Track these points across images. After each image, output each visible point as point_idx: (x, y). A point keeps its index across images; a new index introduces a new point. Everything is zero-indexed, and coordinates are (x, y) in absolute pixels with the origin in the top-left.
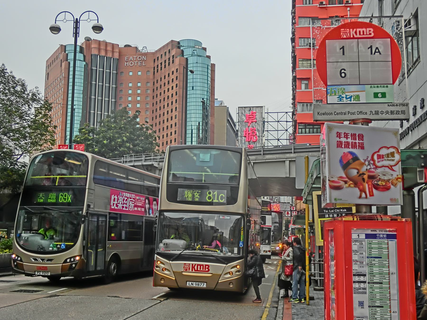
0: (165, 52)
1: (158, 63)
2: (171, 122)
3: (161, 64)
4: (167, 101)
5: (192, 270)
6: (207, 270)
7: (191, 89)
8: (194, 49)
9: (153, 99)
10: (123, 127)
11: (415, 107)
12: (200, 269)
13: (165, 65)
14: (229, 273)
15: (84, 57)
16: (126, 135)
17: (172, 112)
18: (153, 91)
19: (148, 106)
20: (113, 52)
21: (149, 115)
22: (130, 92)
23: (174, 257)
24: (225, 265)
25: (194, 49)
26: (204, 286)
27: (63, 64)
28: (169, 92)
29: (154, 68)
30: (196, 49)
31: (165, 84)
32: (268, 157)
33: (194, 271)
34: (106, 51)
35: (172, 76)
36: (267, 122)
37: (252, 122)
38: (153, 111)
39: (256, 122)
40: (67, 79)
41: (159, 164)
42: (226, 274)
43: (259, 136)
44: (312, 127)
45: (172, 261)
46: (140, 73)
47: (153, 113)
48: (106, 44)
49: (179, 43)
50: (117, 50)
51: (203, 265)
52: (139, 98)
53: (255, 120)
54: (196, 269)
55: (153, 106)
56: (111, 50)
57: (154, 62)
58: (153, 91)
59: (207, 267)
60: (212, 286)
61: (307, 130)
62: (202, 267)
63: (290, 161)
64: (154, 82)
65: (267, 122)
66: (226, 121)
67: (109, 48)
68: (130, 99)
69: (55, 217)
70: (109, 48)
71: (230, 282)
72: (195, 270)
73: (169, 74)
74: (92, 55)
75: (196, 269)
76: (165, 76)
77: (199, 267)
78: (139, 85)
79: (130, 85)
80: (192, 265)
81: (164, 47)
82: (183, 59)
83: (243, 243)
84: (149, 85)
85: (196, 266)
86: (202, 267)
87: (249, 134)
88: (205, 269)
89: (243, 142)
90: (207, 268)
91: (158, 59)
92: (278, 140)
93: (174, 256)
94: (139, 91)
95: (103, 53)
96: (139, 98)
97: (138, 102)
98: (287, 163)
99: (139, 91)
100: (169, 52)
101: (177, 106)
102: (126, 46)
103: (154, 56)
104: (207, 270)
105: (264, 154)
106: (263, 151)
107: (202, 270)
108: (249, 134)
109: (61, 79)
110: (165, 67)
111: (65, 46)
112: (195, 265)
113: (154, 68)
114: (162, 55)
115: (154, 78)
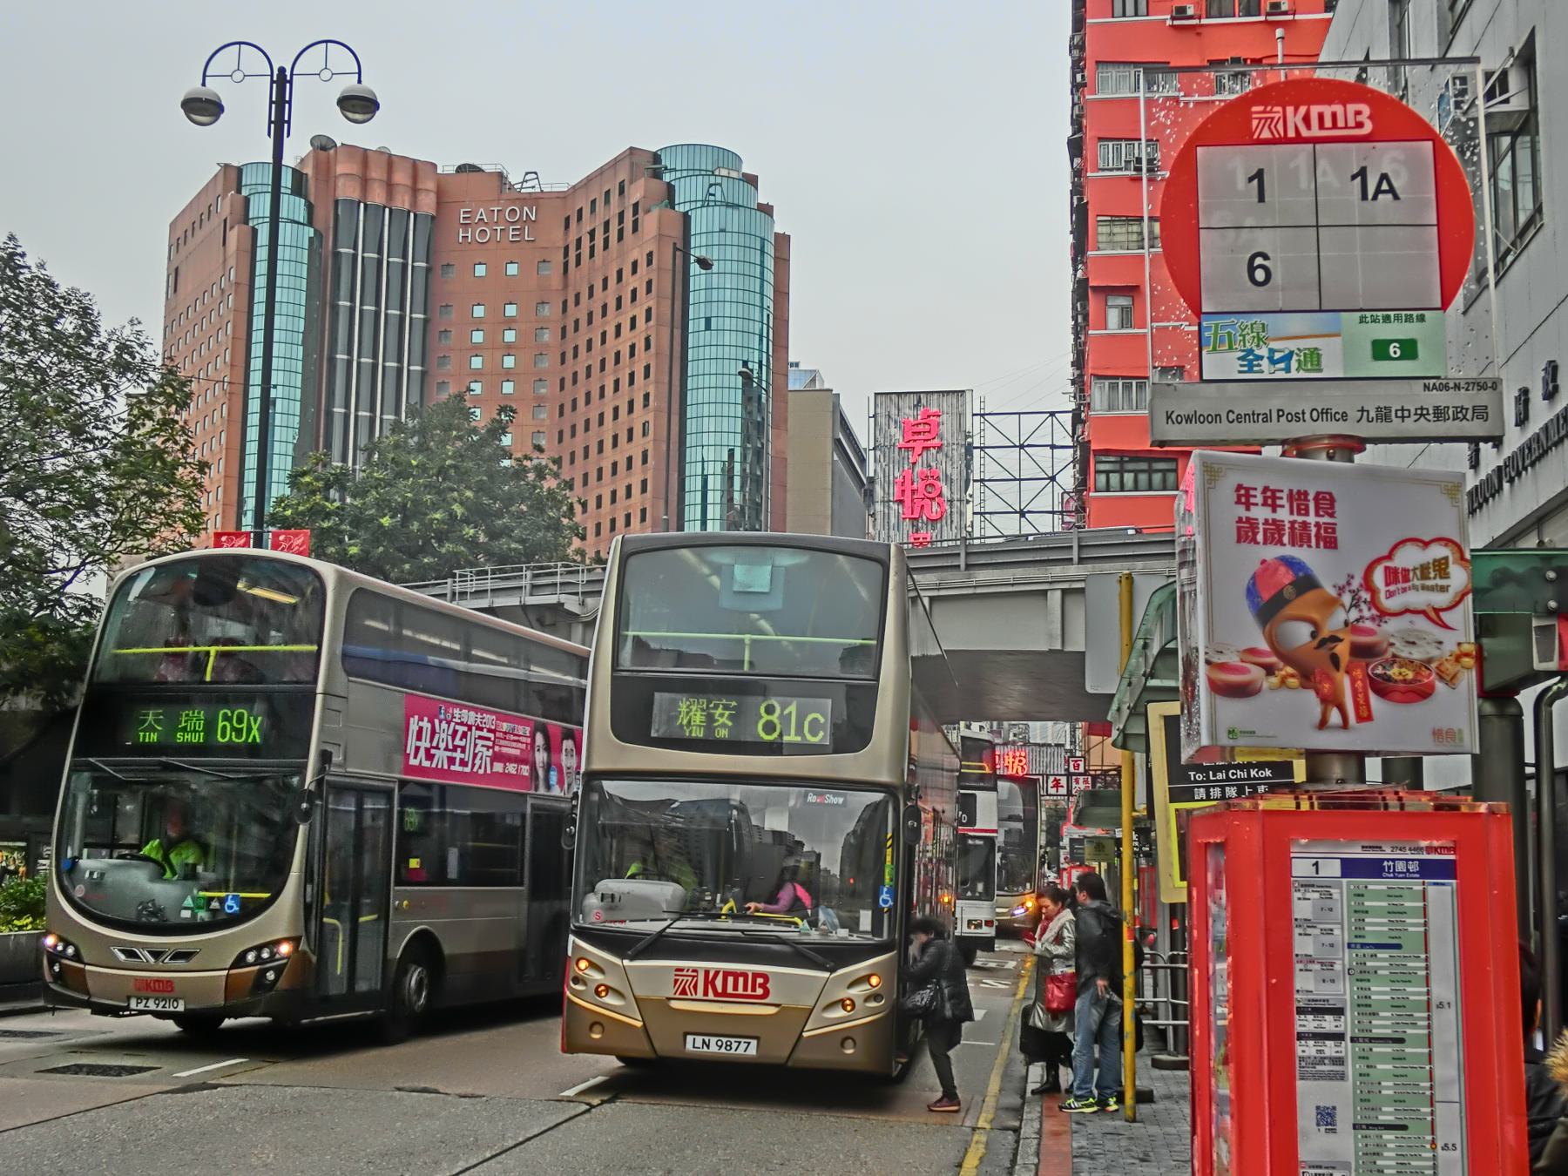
0: (608, 193)
1: (579, 230)
2: (627, 450)
3: (592, 234)
4: (615, 372)
5: (706, 993)
6: (760, 991)
7: (702, 327)
8: (712, 180)
9: (563, 362)
10: (450, 466)
11: (1525, 392)
12: (735, 987)
13: (606, 241)
14: (839, 1005)
15: (310, 208)
16: (461, 495)
17: (631, 410)
18: (564, 336)
19: (543, 391)
20: (415, 191)
21: (547, 422)
22: (478, 337)
23: (640, 946)
24: (826, 975)
25: (712, 180)
26: (750, 1050)
27: (233, 236)
28: (621, 339)
29: (566, 249)
30: (719, 180)
31: (605, 307)
32: (983, 575)
33: (711, 996)
34: (390, 186)
35: (631, 279)
36: (981, 448)
37: (927, 448)
38: (562, 407)
39: (940, 448)
40: (245, 290)
41: (583, 604)
42: (830, 1006)
43: (951, 501)
44: (1144, 466)
45: (632, 959)
46: (512, 269)
47: (561, 414)
48: (390, 161)
49: (656, 157)
50: (430, 185)
51: (745, 975)
52: (509, 362)
53: (936, 441)
54: (720, 990)
55: (562, 388)
56: (409, 182)
57: (567, 226)
58: (564, 336)
59: (760, 980)
60: (780, 1053)
61: (1129, 478)
62: (741, 980)
63: (1064, 592)
64: (565, 303)
65: (981, 448)
66: (829, 445)
67: (401, 177)
68: (477, 363)
69: (204, 798)
70: (401, 177)
71: (845, 1038)
72: (716, 993)
73: (620, 273)
74: (336, 202)
75: (720, 990)
76: (605, 281)
77: (731, 980)
78: (511, 311)
79: (479, 311)
80: (707, 972)
81: (601, 172)
82: (673, 217)
83: (893, 893)
84: (546, 311)
85: (720, 977)
86: (741, 980)
87: (913, 491)
88: (754, 989)
89: (893, 520)
90: (761, 986)
91: (580, 218)
92: (1022, 514)
93: (640, 940)
94: (510, 336)
95: (377, 196)
96: (509, 362)
97: (508, 375)
98: (1055, 598)
99: (510, 336)
100: (622, 192)
101: (651, 390)
102: (461, 169)
103: (567, 207)
104: (760, 991)
105: (968, 567)
106: (968, 554)
107: (740, 991)
108: (913, 491)
109: (223, 291)
110: (606, 247)
111: (239, 170)
112: (717, 973)
113: (566, 249)
114: (593, 202)
115: (566, 286)
